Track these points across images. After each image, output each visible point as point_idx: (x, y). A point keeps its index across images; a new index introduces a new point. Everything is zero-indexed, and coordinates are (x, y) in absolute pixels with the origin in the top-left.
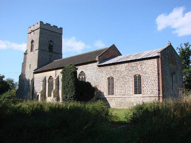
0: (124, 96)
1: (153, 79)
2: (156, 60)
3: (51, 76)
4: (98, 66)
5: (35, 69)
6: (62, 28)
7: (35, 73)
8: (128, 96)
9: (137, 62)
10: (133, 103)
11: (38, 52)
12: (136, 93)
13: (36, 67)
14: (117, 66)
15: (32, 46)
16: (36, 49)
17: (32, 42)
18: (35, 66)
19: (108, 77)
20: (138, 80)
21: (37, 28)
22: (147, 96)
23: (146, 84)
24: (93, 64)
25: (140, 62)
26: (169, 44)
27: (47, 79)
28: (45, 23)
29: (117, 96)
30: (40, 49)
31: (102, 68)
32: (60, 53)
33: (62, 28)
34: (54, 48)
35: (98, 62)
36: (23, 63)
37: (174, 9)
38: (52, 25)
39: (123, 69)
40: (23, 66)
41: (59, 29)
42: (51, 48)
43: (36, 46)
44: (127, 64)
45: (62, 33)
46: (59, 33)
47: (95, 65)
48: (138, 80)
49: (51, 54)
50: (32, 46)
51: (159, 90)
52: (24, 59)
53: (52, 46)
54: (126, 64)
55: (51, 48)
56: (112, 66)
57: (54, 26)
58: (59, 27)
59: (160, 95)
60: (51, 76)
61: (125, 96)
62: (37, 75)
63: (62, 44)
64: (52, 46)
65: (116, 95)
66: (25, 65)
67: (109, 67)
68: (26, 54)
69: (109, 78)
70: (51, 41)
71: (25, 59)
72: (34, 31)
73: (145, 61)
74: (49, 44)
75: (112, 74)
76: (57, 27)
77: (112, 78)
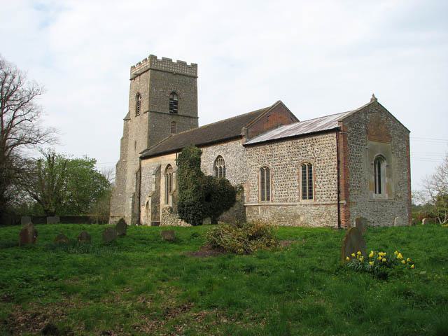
0: (285, 204)
1: (330, 170)
2: (335, 135)
3: (169, 165)
4: (244, 146)
5: (142, 150)
6: (196, 65)
7: (142, 158)
8: (291, 204)
9: (306, 139)
10: (297, 217)
11: (147, 116)
12: (304, 198)
13: (145, 147)
14: (274, 146)
15: (138, 103)
16: (145, 111)
17: (138, 95)
18: (143, 145)
19: (260, 166)
20: (308, 172)
21: (147, 69)
22: (320, 203)
23: (319, 180)
24: (232, 144)
25: (311, 138)
26: (374, 101)
27: (163, 169)
28: (160, 58)
29: (274, 204)
30: (153, 112)
31: (251, 149)
32: (194, 116)
33: (196, 65)
34: (180, 105)
35: (244, 139)
36: (122, 139)
37: (27, 152)
38: (174, 61)
39: (285, 152)
40: (122, 144)
41: (188, 67)
42: (173, 106)
43: (145, 106)
44: (290, 142)
45: (196, 73)
46: (190, 76)
47: (238, 145)
48: (308, 172)
49: (174, 120)
50: (138, 103)
51: (339, 192)
52: (125, 130)
53: (176, 103)
54: (289, 143)
55: (173, 106)
56: (267, 147)
57: (179, 62)
58: (189, 64)
59: (341, 202)
60: (169, 165)
61: (287, 204)
62: (145, 162)
63: (197, 97)
64: (176, 103)
65: (272, 201)
66: (127, 142)
67: (260, 149)
68: (126, 120)
69: (262, 168)
70: (174, 93)
71: (126, 129)
72: (140, 75)
73: (319, 137)
74: (171, 99)
75: (266, 162)
76: (184, 64)
77: (268, 170)
